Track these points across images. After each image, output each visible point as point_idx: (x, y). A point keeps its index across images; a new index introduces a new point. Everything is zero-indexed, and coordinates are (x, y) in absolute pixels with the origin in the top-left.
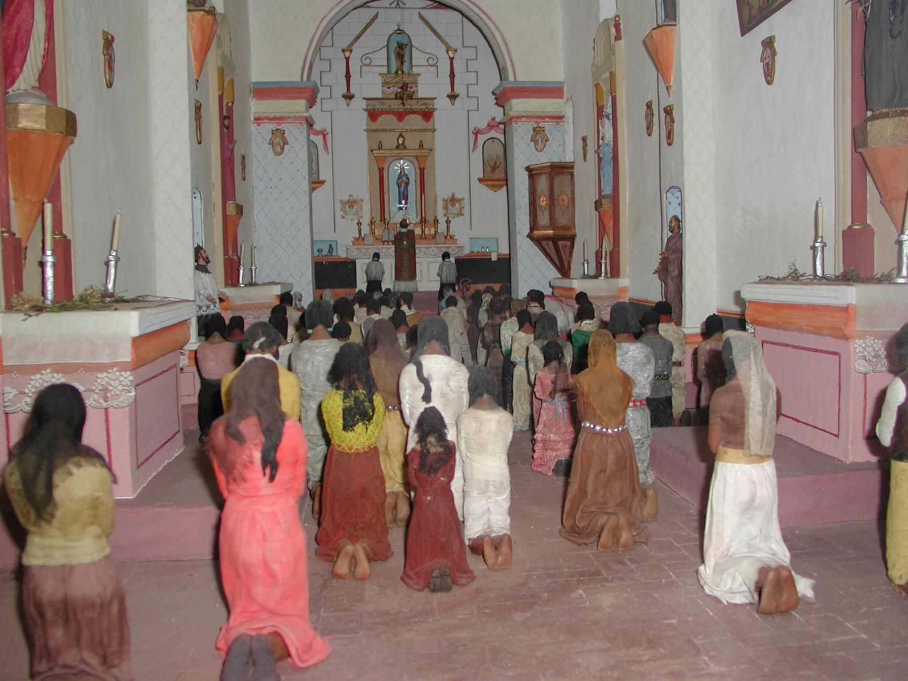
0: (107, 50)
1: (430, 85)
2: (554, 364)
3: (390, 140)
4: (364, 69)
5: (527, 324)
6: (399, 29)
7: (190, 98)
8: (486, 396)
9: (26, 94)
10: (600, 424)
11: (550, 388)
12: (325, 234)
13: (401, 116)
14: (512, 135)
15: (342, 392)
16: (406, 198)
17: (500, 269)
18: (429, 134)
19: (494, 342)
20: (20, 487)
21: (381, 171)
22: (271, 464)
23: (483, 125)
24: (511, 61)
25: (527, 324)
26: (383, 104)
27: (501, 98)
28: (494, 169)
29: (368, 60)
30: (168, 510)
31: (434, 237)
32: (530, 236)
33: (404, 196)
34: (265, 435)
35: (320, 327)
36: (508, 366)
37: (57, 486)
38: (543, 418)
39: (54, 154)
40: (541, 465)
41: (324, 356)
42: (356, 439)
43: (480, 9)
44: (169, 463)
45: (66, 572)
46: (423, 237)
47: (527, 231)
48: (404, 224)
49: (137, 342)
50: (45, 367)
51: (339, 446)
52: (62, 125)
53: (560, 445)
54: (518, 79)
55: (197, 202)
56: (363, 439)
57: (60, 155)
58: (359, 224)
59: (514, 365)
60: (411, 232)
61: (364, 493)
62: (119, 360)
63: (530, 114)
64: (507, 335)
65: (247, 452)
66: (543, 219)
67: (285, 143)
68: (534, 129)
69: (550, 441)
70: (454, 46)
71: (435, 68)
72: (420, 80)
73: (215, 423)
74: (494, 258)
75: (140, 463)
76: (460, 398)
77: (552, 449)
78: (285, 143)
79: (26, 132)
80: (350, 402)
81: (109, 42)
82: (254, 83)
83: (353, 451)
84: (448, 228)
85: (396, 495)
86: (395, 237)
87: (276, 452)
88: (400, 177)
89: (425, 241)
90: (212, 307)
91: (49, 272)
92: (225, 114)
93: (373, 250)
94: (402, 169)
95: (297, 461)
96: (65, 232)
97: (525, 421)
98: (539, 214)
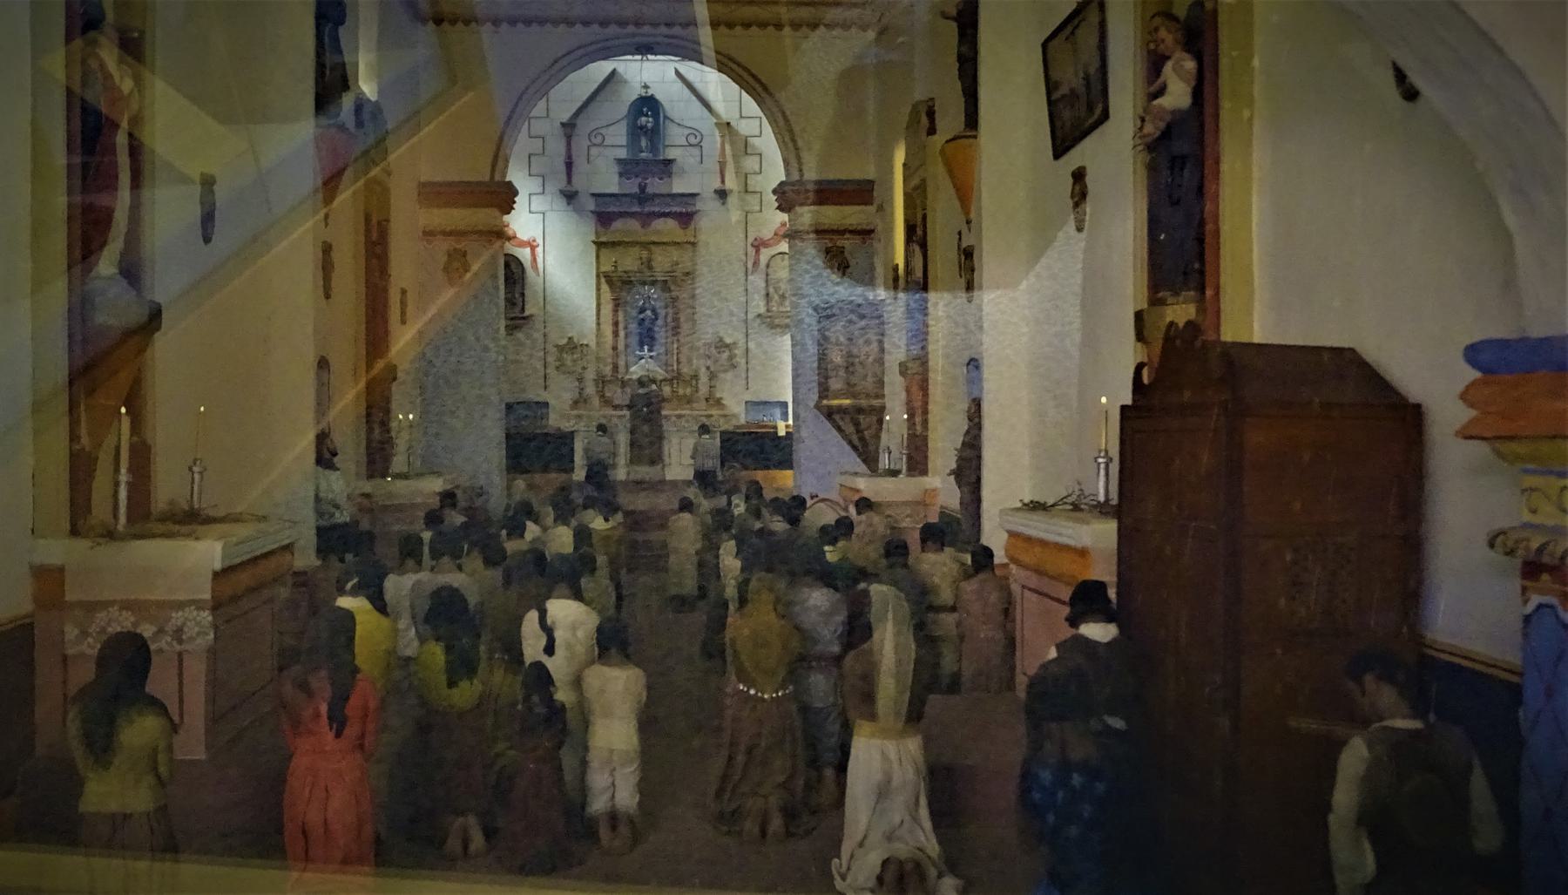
4: (594, 151)
10: (754, 686)
32: (818, 407)
35: (446, 559)
71: (696, 151)
91: (123, 494)
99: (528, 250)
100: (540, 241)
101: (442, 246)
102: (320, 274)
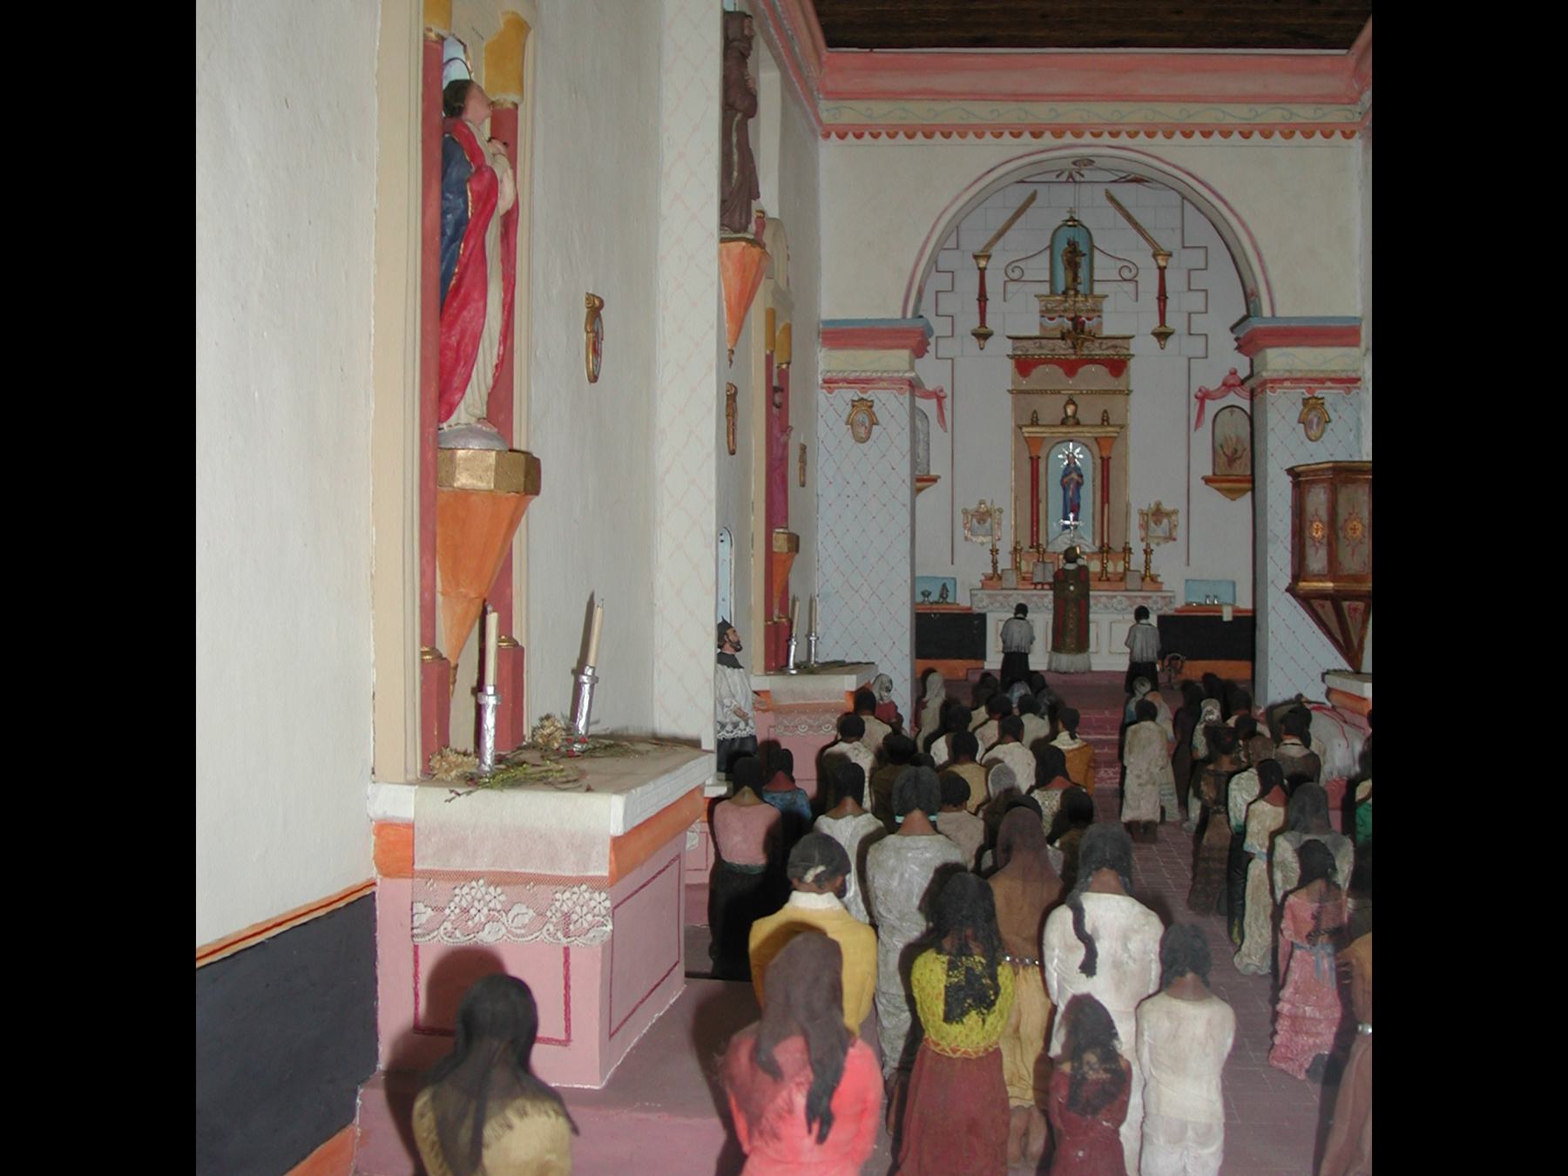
0: (593, 323)
1: (1122, 314)
2: (1318, 885)
3: (1051, 409)
4: (1011, 287)
5: (1276, 788)
6: (1072, 219)
8: (1190, 976)
9: (470, 432)
11: (1308, 927)
12: (935, 565)
13: (1071, 368)
14: (1265, 411)
15: (945, 958)
16: (1075, 509)
17: (1240, 636)
18: (1119, 399)
19: (1216, 802)
20: (433, 1137)
21: (1034, 461)
22: (820, 1116)
23: (1214, 384)
24: (1267, 283)
25: (1276, 788)
26: (1041, 347)
27: (1250, 340)
28: (1231, 460)
29: (1018, 272)
30: (653, 1117)
31: (1122, 578)
33: (1072, 506)
34: (814, 1071)
35: (917, 814)
36: (1238, 859)
37: (488, 1147)
38: (1294, 976)
39: (505, 524)
40: (1286, 1059)
41: (922, 865)
42: (964, 1037)
43: (1214, 193)
44: (660, 1019)
46: (1104, 577)
47: (1286, 580)
48: (1070, 555)
49: (618, 843)
50: (476, 876)
51: (937, 1045)
52: (519, 480)
53: (1322, 1027)
54: (1278, 314)
55: (725, 548)
57: (513, 525)
58: (994, 551)
59: (1250, 857)
60: (1084, 569)
61: (973, 1127)
62: (590, 873)
63: (1299, 375)
64: (1239, 800)
65: (784, 1094)
66: (1317, 561)
67: (874, 423)
68: (1305, 402)
69: (1304, 1018)
70: (1166, 247)
71: (1131, 286)
72: (1107, 306)
73: (735, 1038)
74: (1227, 616)
75: (615, 1025)
76: (1146, 970)
77: (1306, 1033)
78: (874, 423)
79: (466, 493)
80: (959, 977)
81: (595, 310)
82: (826, 322)
83: (958, 1054)
84: (1147, 563)
85: (1028, 1111)
86: (1056, 576)
87: (830, 1098)
88: (1067, 472)
89: (1105, 585)
90: (742, 725)
92: (775, 383)
93: (1018, 598)
94: (1071, 458)
95: (863, 1111)
96: (515, 636)
97: (1264, 957)
98: (1310, 551)
99: (934, 401)
100: (948, 391)
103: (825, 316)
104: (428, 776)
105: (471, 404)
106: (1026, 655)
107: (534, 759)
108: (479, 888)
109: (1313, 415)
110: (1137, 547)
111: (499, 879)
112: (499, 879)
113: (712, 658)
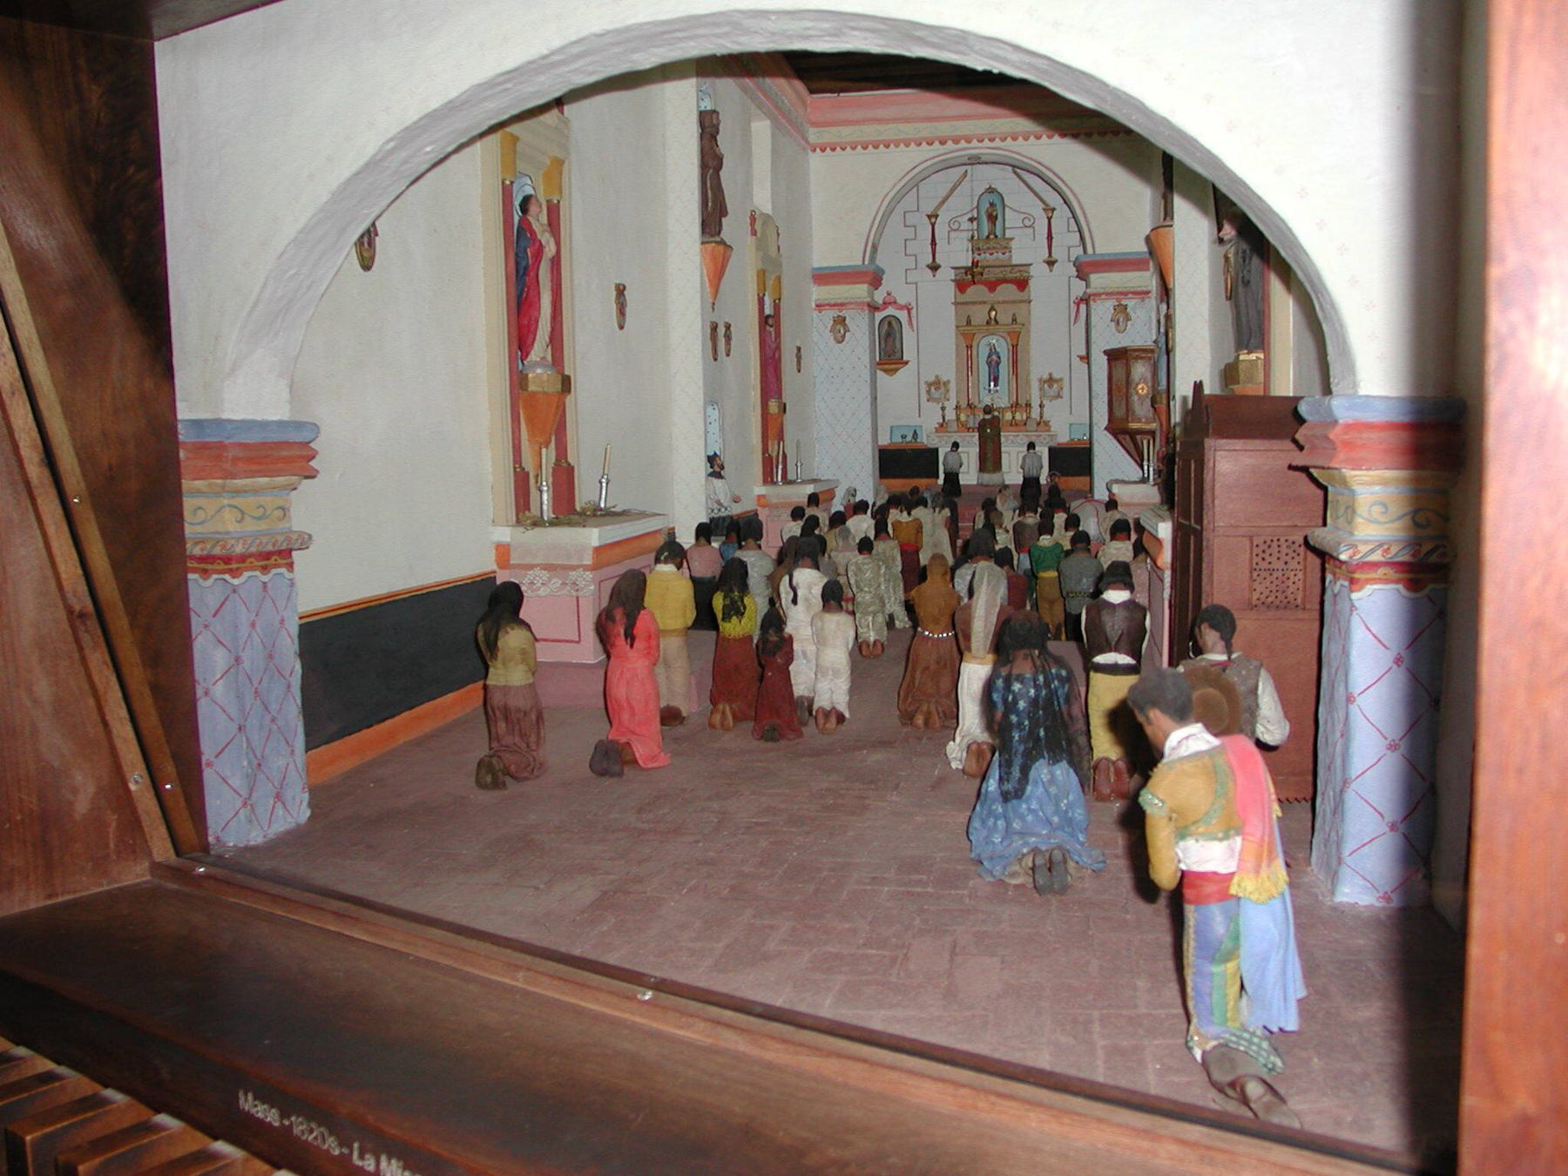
1: (1025, 249)
3: (980, 315)
4: (953, 234)
7: (703, 320)
16: (996, 380)
27: (1083, 270)
45: (506, 689)
49: (597, 550)
55: (714, 414)
56: (738, 629)
72: (1013, 244)
81: (621, 291)
92: (768, 311)
101: (830, 314)
102: (709, 343)
103: (816, 265)
104: (519, 522)
105: (540, 348)
106: (957, 475)
107: (567, 511)
108: (537, 571)
109: (1121, 315)
110: (1035, 404)
111: (548, 567)
112: (548, 567)
113: (703, 474)
